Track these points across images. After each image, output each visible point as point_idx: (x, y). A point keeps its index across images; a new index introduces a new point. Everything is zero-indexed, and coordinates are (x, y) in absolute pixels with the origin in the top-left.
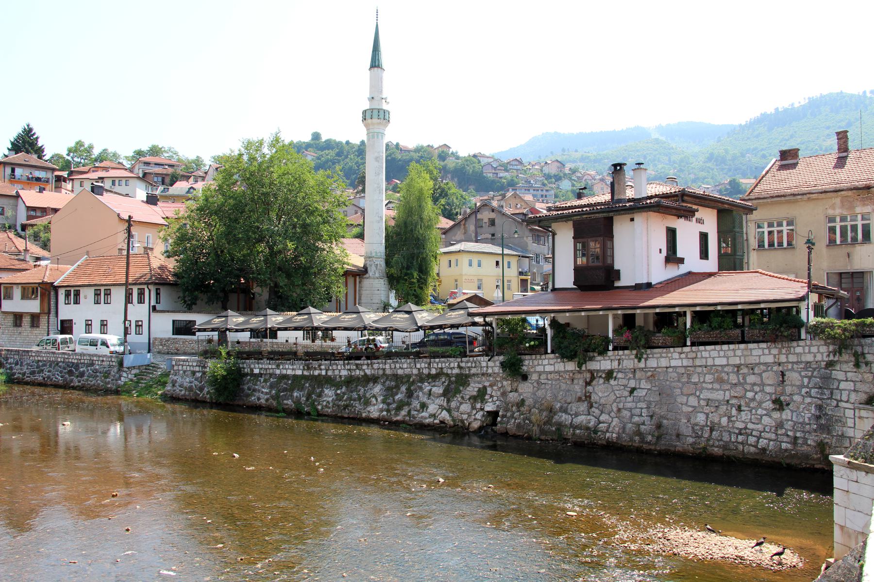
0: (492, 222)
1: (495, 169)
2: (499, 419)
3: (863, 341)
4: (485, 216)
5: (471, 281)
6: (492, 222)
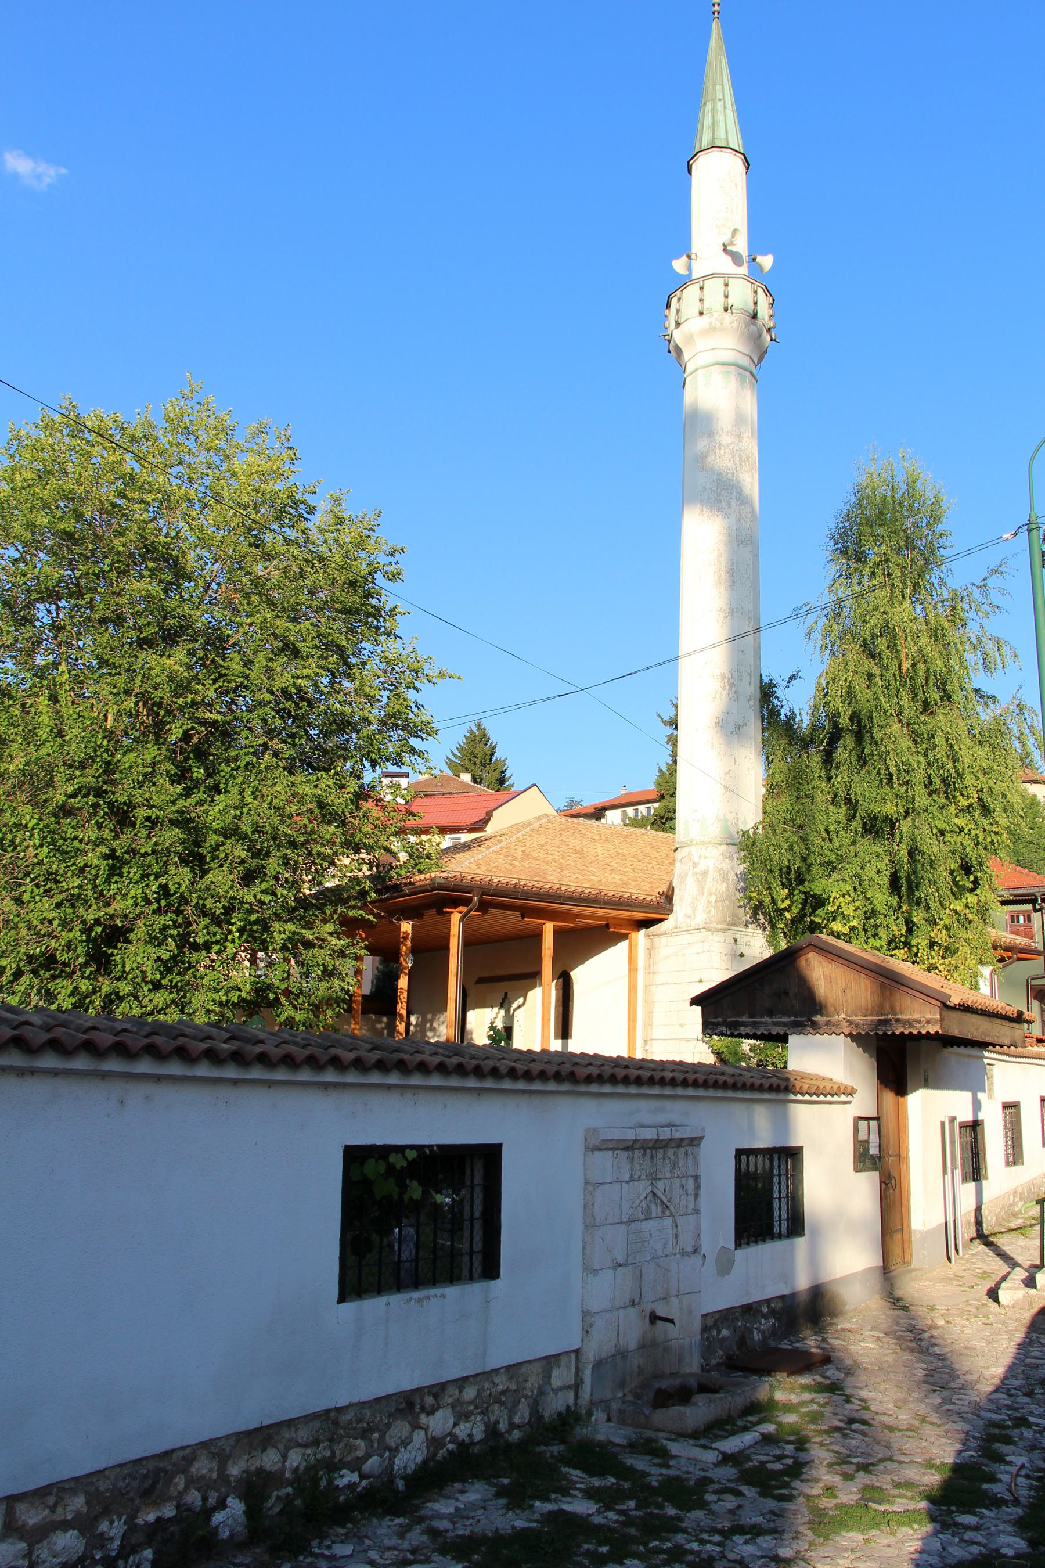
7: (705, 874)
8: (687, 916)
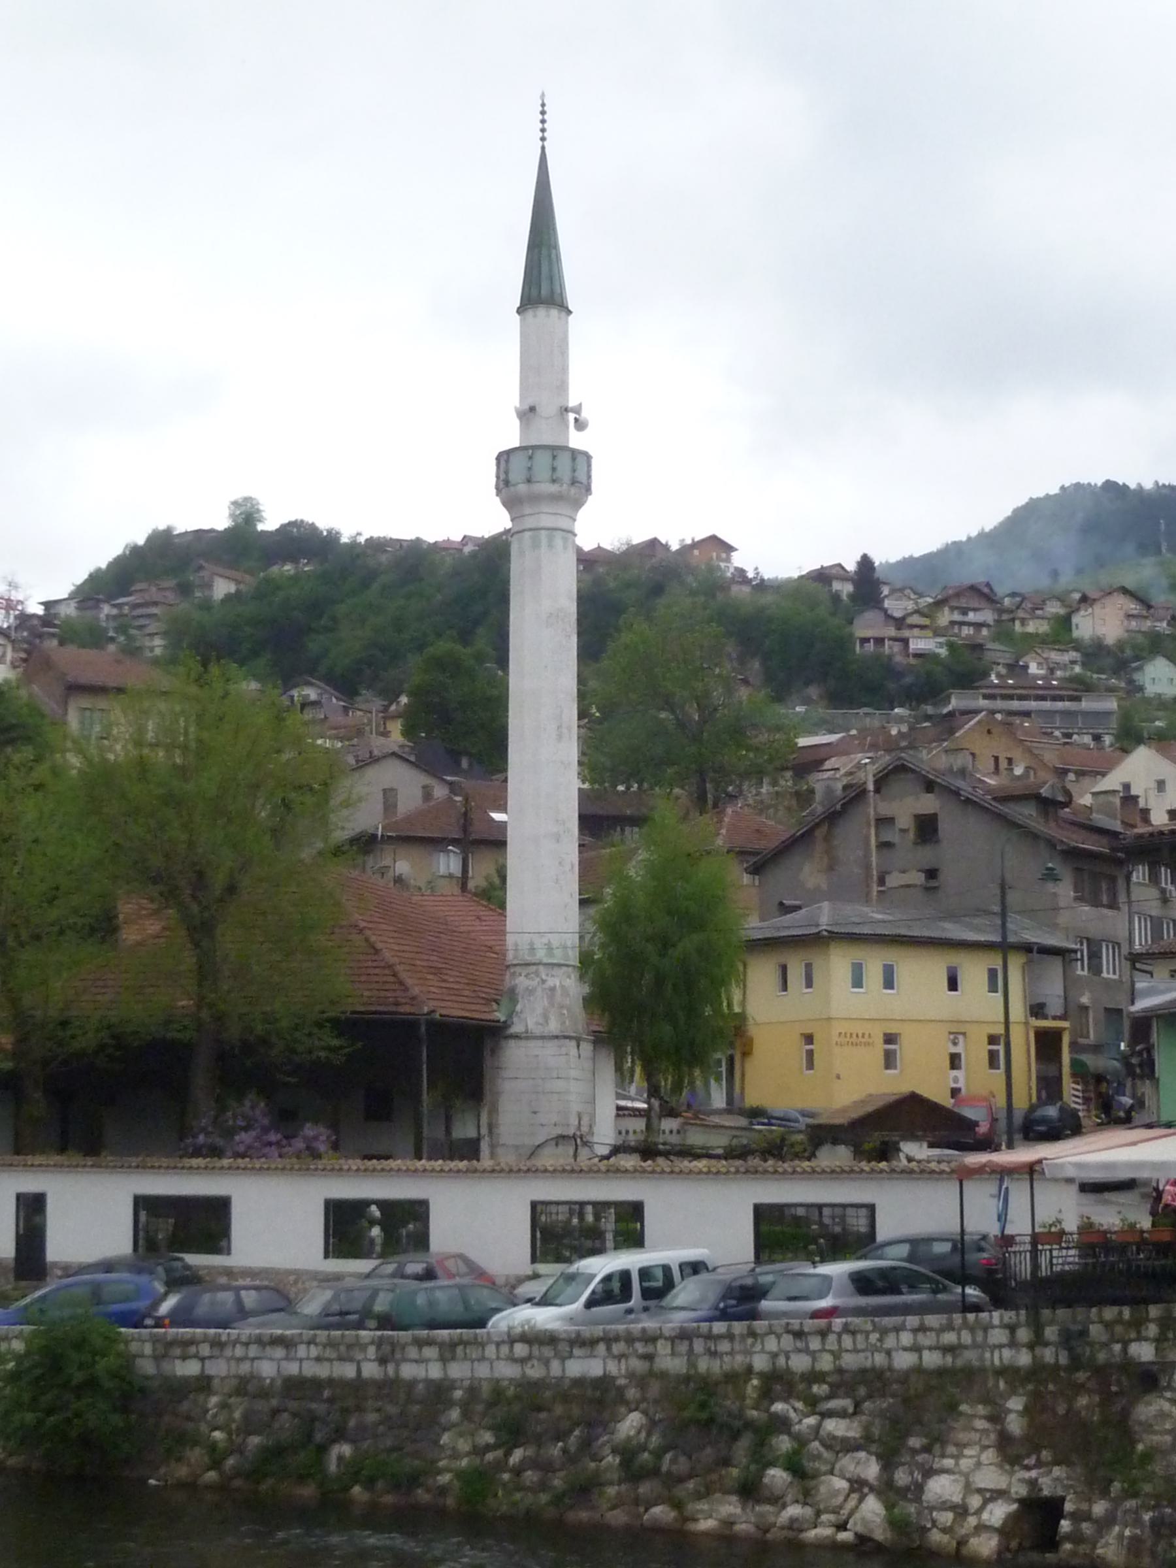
0: (927, 828)
1: (900, 623)
2: (1065, 1525)
3: (1117, 826)
4: (905, 806)
5: (857, 1041)
6: (927, 828)
7: (553, 989)
8: (537, 1024)
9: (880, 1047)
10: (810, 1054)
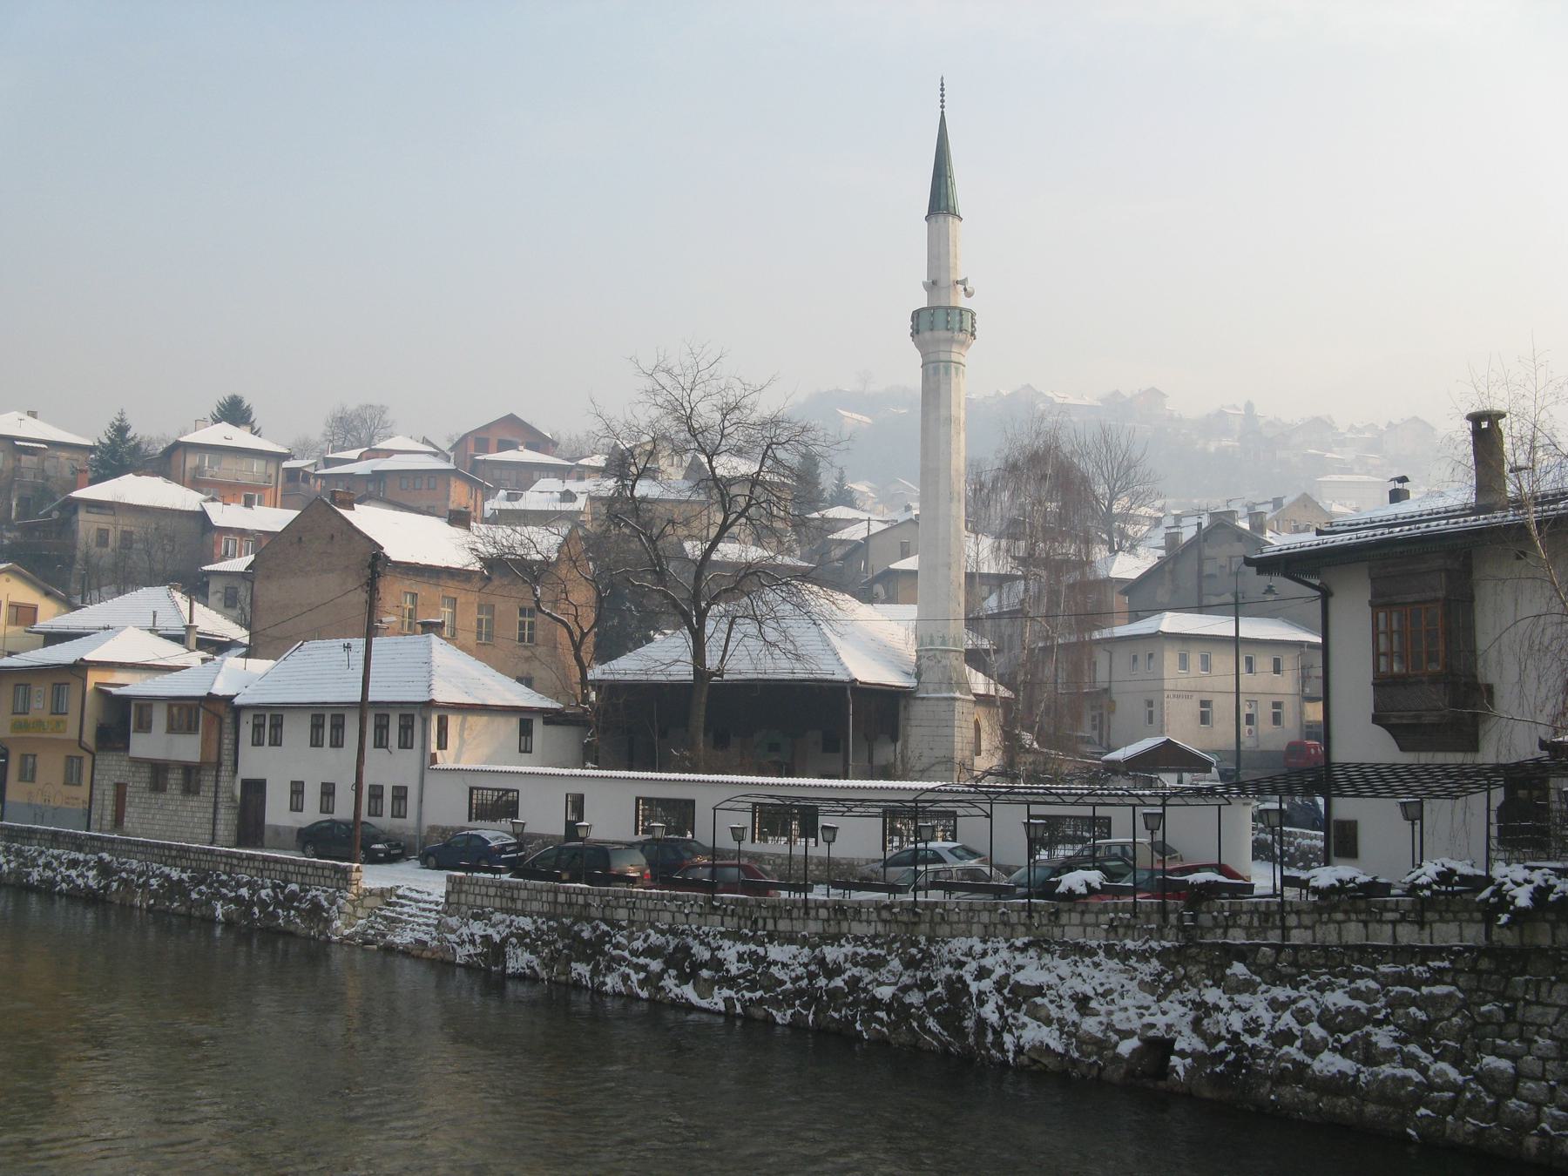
9: (1197, 709)
10: (1151, 713)
